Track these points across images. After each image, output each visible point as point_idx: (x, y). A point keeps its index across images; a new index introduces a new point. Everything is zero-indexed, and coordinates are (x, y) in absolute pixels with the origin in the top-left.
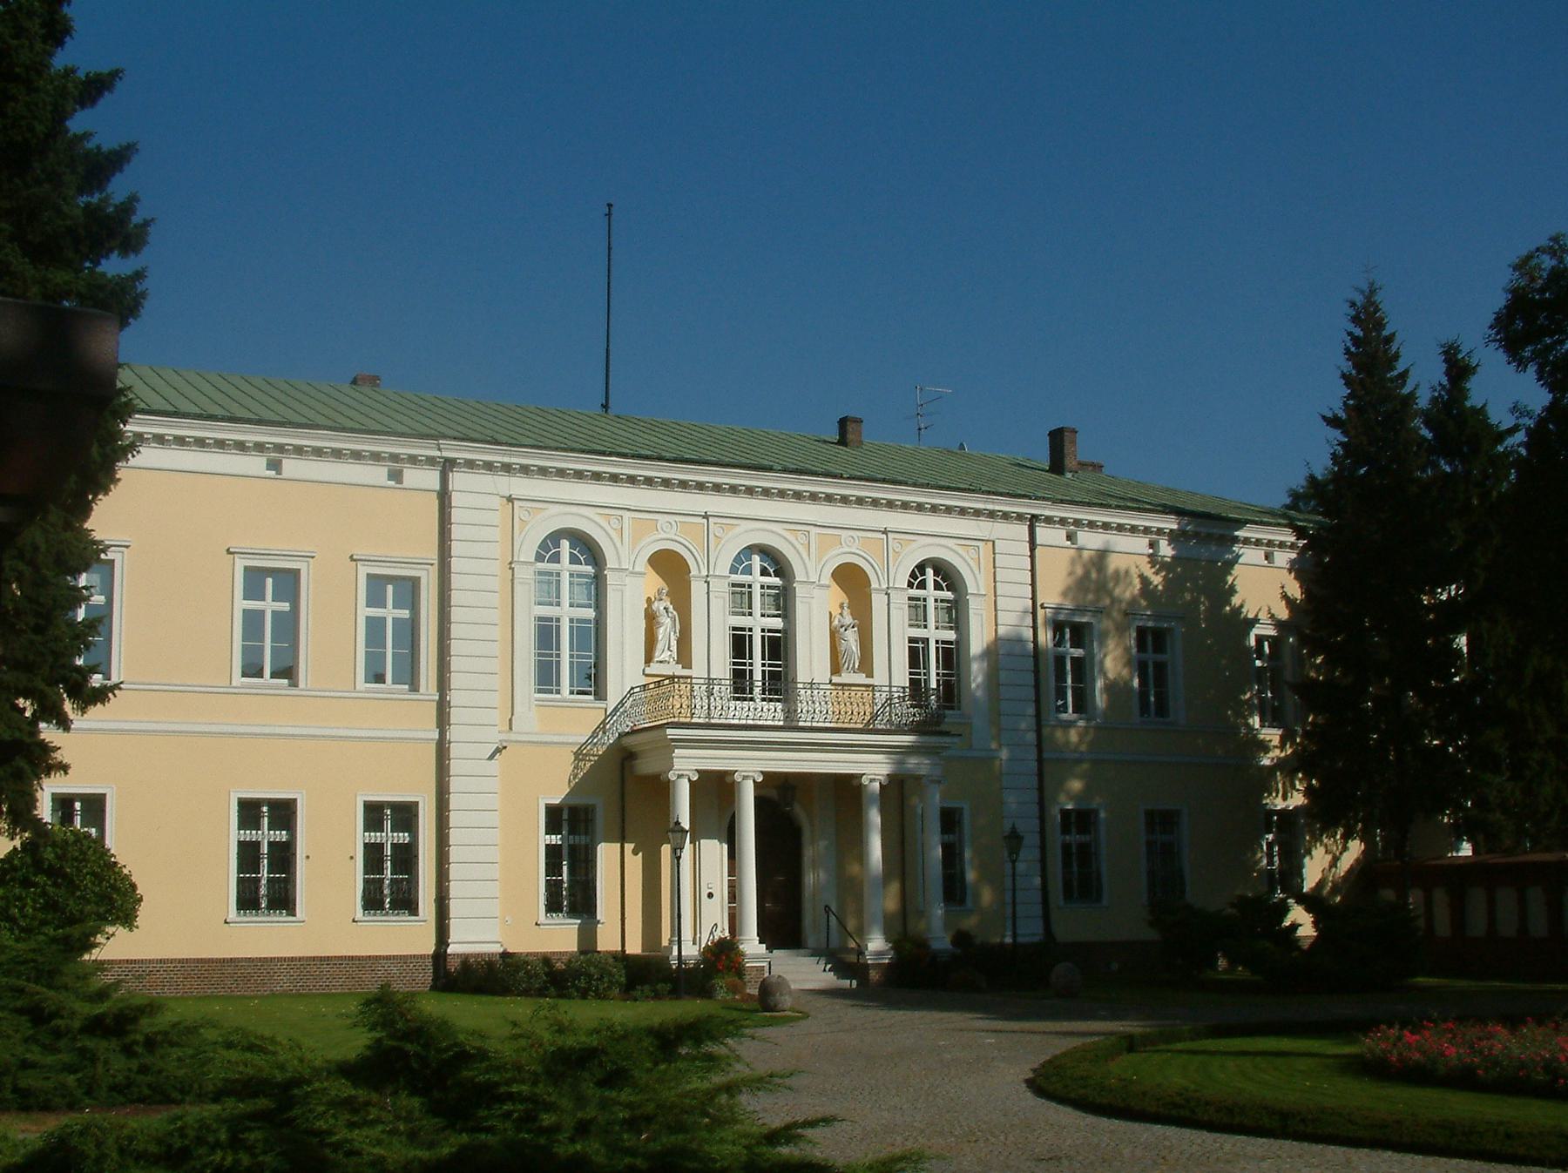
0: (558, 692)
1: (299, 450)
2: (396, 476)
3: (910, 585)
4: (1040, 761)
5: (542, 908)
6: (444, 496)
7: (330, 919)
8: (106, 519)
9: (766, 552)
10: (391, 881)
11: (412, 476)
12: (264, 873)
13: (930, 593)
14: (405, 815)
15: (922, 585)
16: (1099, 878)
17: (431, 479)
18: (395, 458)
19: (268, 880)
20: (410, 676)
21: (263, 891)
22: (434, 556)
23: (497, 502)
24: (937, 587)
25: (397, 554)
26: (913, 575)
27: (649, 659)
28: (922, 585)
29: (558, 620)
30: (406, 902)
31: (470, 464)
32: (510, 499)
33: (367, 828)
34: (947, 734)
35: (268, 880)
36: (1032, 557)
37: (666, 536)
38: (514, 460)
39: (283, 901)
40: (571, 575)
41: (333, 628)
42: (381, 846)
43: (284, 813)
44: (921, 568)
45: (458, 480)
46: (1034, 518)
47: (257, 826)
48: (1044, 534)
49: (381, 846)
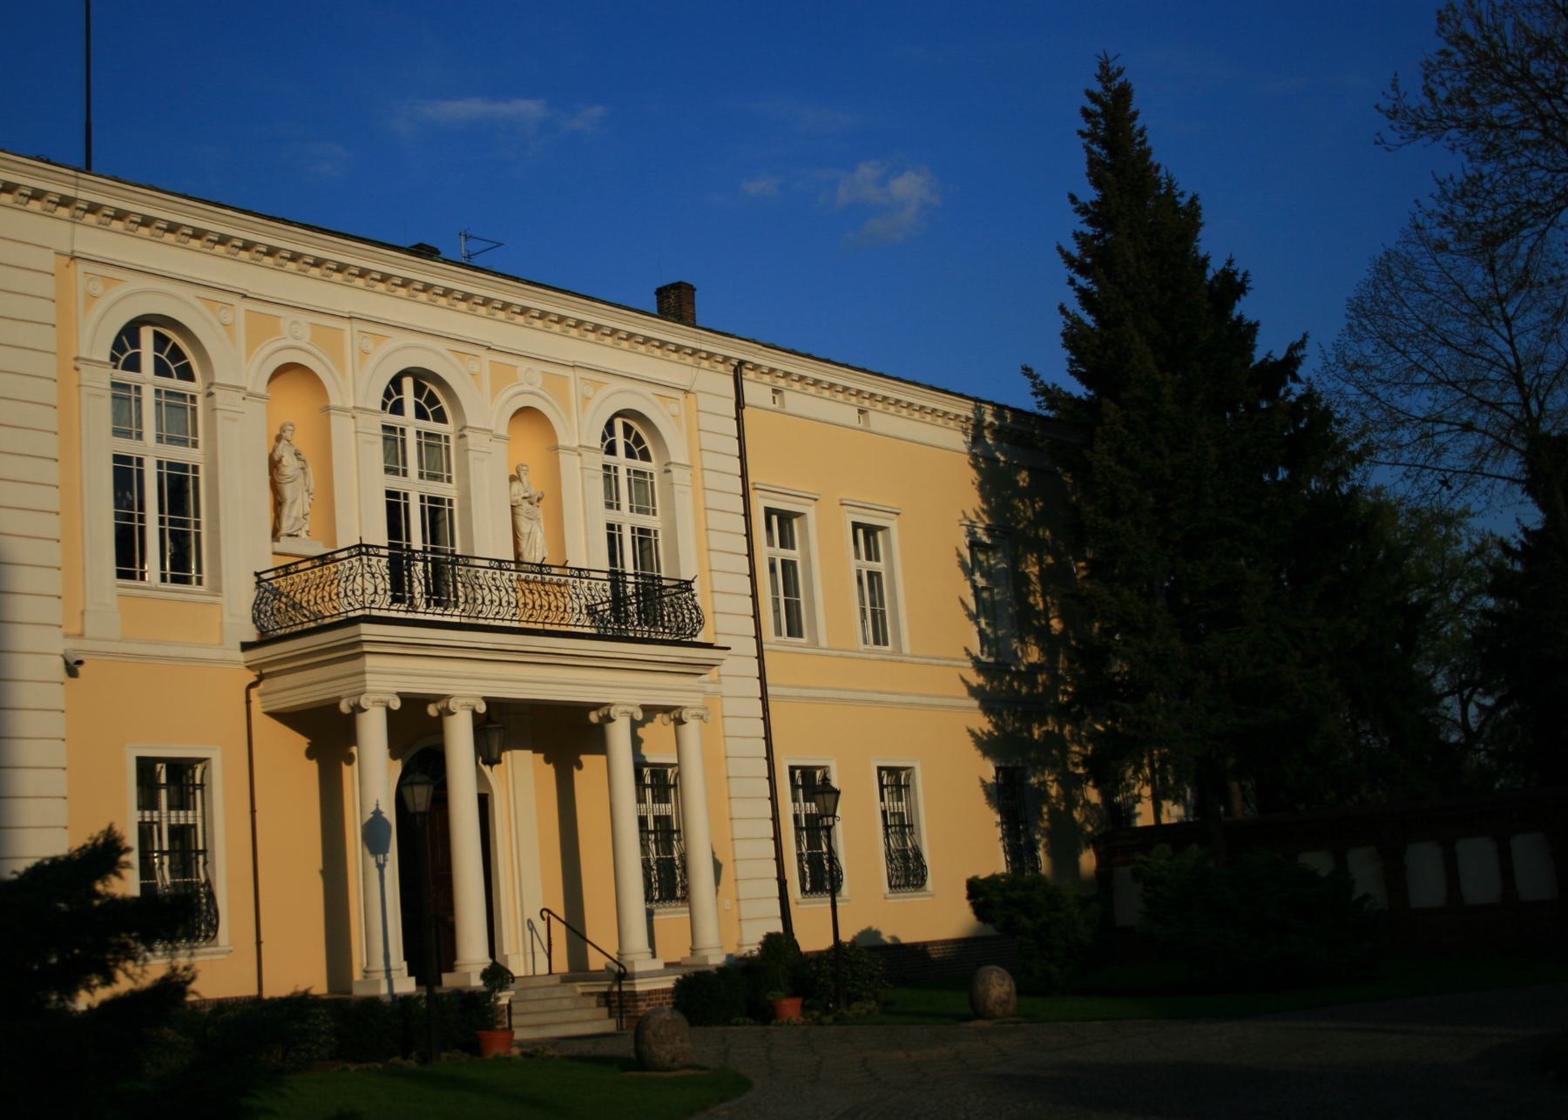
3: (384, 406)
4: (764, 698)
13: (409, 421)
16: (211, 896)
23: (48, 261)
27: (276, 534)
29: (140, 461)
33: (142, 807)
34: (709, 646)
36: (739, 419)
38: (82, 195)
44: (130, 332)
46: (742, 363)
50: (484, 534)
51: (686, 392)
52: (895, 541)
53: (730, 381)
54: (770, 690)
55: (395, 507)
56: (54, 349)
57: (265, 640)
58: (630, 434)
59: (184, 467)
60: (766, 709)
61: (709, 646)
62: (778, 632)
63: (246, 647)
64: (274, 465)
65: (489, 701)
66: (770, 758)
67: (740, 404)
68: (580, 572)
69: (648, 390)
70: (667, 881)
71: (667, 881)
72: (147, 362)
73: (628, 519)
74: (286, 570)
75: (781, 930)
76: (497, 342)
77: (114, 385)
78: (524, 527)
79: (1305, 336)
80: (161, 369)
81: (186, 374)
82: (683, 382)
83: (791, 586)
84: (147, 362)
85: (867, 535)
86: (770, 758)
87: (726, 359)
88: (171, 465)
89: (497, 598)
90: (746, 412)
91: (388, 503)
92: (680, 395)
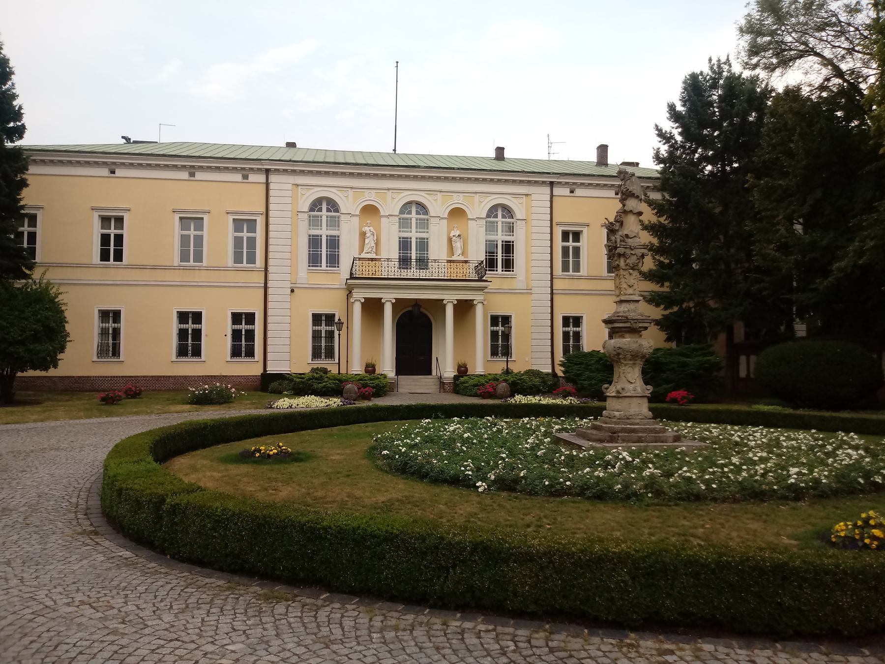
1: (201, 167)
2: (245, 177)
4: (552, 294)
5: (310, 357)
6: (267, 184)
7: (216, 359)
8: (28, 197)
9: (419, 204)
10: (242, 343)
11: (252, 178)
12: (571, 342)
14: (250, 318)
19: (189, 343)
20: (252, 259)
21: (190, 348)
22: (263, 210)
23: (290, 187)
25: (246, 210)
30: (250, 353)
31: (277, 170)
34: (486, 281)
35: (189, 343)
36: (551, 202)
37: (457, 201)
39: (197, 352)
41: (219, 241)
42: (569, 332)
43: (197, 317)
47: (569, 326)
48: (557, 191)
49: (569, 332)
50: (437, 251)
51: (527, 195)
52: (584, 238)
61: (486, 281)
62: (565, 268)
67: (552, 196)
69: (422, 193)
73: (414, 235)
81: (337, 211)
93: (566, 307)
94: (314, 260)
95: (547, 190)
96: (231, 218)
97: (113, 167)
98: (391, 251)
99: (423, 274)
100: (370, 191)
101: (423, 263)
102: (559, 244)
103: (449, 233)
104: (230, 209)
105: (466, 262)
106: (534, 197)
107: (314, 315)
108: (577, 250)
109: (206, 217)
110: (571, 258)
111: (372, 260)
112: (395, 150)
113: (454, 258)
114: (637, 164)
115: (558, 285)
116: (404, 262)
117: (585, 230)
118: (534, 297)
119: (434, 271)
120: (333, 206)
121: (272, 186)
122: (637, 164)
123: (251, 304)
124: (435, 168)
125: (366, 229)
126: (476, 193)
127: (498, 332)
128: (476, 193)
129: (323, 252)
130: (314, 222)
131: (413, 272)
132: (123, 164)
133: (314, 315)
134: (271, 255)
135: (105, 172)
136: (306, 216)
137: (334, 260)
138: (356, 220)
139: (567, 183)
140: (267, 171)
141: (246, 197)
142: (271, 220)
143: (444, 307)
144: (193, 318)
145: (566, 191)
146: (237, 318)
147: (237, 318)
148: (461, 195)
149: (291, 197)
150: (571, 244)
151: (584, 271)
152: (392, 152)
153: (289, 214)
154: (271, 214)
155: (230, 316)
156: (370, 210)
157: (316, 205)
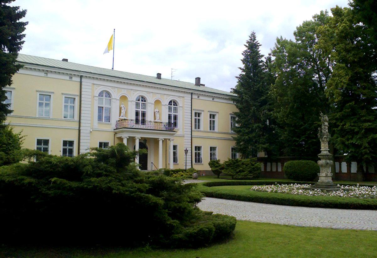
0: (102, 121)
3: (169, 104)
4: (192, 137)
6: (81, 82)
11: (74, 79)
14: (71, 143)
15: (171, 105)
17: (79, 79)
18: (71, 74)
22: (79, 94)
23: (91, 85)
24: (174, 105)
26: (170, 103)
27: (120, 116)
28: (171, 105)
32: (94, 84)
33: (195, 150)
34: (175, 131)
37: (124, 93)
38: (94, 77)
40: (106, 99)
42: (66, 149)
43: (46, 142)
44: (171, 102)
45: (83, 80)
47: (196, 150)
49: (66, 149)
50: (149, 117)
51: (183, 97)
52: (216, 117)
53: (80, 79)
54: (192, 136)
55: (137, 114)
56: (91, 95)
57: (117, 129)
58: (173, 103)
59: (176, 115)
60: (192, 139)
61: (175, 131)
62: (195, 128)
63: (114, 130)
64: (121, 108)
65: (129, 137)
66: (192, 145)
67: (192, 98)
68: (150, 122)
69: (176, 97)
70: (175, 160)
71: (175, 160)
72: (141, 100)
74: (119, 121)
75: (335, 163)
76: (153, 92)
77: (169, 107)
78: (156, 115)
79: (239, 68)
80: (174, 105)
81: (176, 105)
82: (183, 96)
83: (199, 122)
84: (141, 100)
85: (212, 116)
86: (192, 145)
87: (78, 75)
88: (143, 112)
89: (148, 126)
90: (193, 99)
91: (169, 116)
92: (182, 98)
93: (196, 143)
94: (100, 118)
95: (190, 96)
96: (64, 96)
97: (199, 95)
98: (132, 116)
99: (144, 127)
100: (124, 90)
101: (143, 122)
102: (194, 117)
103: (154, 110)
104: (38, 89)
105: (161, 123)
106: (185, 98)
107: (64, 141)
108: (214, 121)
109: (52, 95)
110: (197, 124)
111: (124, 119)
112: (113, 68)
113: (156, 121)
114: (204, 85)
115: (194, 134)
116: (137, 121)
117: (203, 113)
118: (185, 138)
119: (148, 126)
120: (108, 94)
121: (83, 83)
122: (204, 85)
123: (72, 137)
124: (41, 65)
125: (122, 106)
126: (165, 94)
127: (66, 149)
128: (165, 94)
129: (103, 114)
130: (100, 101)
131: (140, 126)
132: (51, 72)
133: (64, 141)
134: (82, 115)
135: (67, 78)
136: (97, 98)
137: (108, 119)
138: (118, 102)
139: (197, 94)
140: (81, 77)
141: (72, 88)
142: (82, 99)
143: (158, 141)
144: (44, 142)
145: (196, 97)
146: (65, 143)
147: (65, 143)
148: (126, 90)
149: (91, 90)
150: (197, 118)
151: (216, 130)
152: (111, 69)
153: (90, 97)
154: (83, 96)
155: (62, 142)
156: (124, 98)
157: (101, 94)
